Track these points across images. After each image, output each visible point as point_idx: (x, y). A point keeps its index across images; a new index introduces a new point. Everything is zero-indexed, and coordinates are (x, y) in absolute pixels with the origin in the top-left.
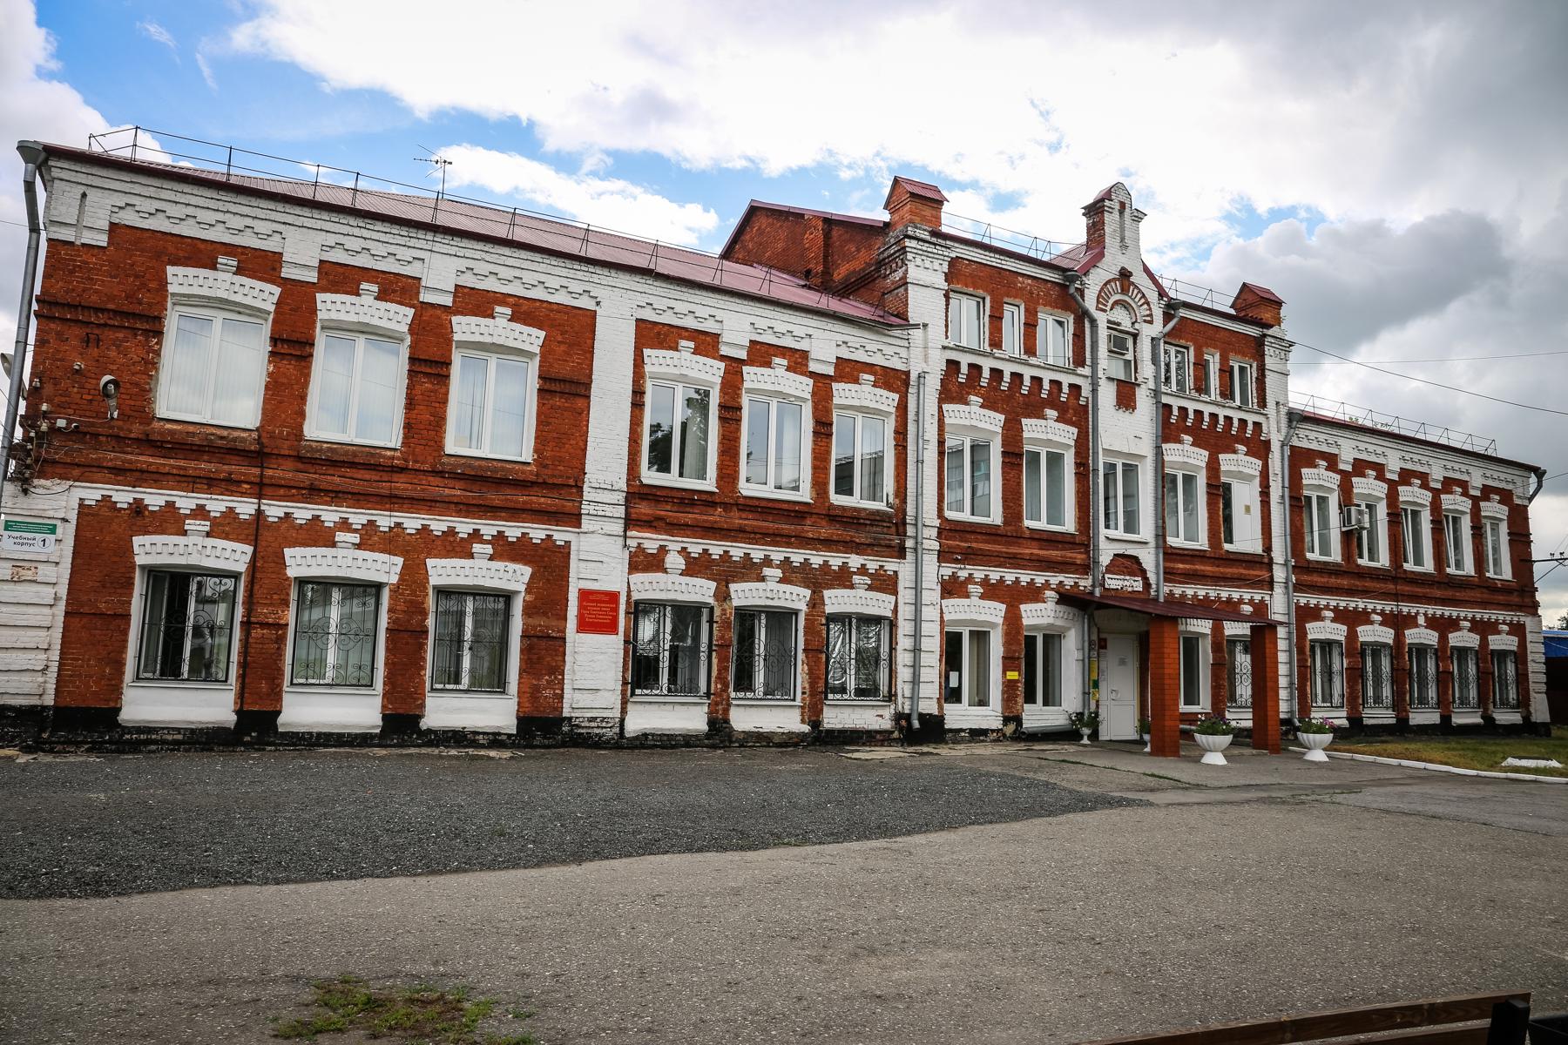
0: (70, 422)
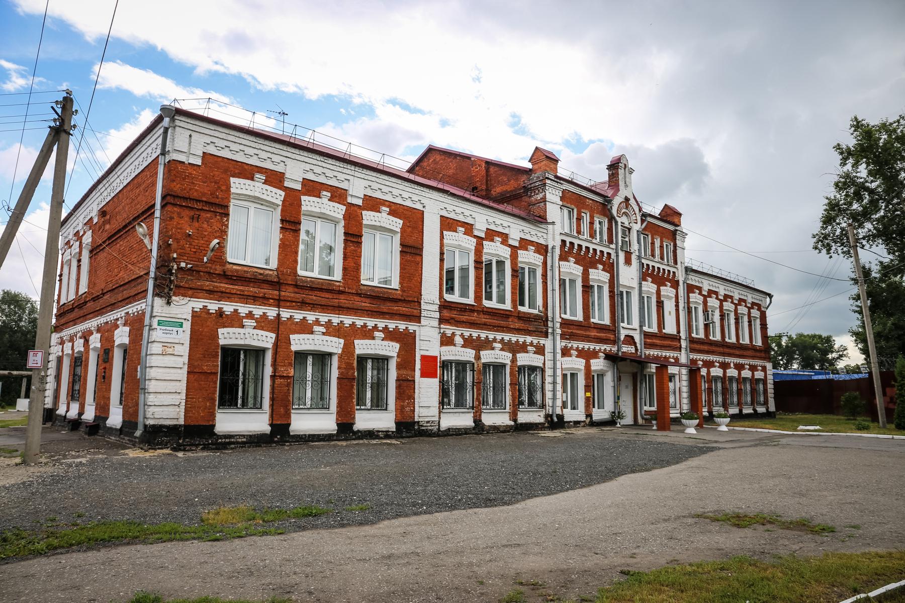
0: (187, 264)
